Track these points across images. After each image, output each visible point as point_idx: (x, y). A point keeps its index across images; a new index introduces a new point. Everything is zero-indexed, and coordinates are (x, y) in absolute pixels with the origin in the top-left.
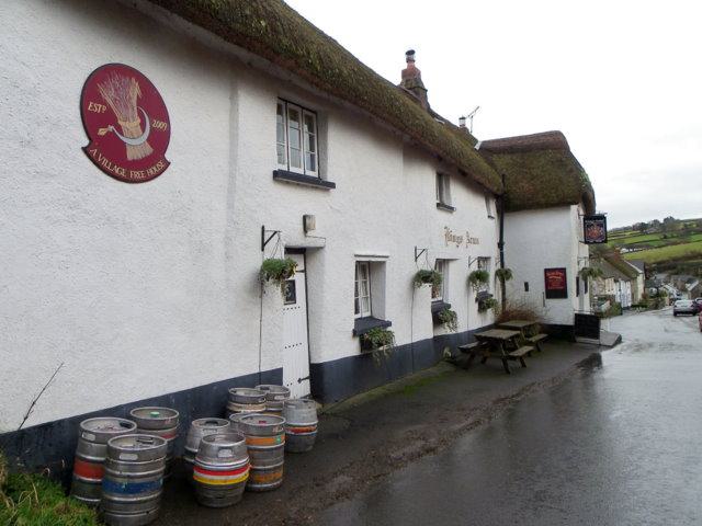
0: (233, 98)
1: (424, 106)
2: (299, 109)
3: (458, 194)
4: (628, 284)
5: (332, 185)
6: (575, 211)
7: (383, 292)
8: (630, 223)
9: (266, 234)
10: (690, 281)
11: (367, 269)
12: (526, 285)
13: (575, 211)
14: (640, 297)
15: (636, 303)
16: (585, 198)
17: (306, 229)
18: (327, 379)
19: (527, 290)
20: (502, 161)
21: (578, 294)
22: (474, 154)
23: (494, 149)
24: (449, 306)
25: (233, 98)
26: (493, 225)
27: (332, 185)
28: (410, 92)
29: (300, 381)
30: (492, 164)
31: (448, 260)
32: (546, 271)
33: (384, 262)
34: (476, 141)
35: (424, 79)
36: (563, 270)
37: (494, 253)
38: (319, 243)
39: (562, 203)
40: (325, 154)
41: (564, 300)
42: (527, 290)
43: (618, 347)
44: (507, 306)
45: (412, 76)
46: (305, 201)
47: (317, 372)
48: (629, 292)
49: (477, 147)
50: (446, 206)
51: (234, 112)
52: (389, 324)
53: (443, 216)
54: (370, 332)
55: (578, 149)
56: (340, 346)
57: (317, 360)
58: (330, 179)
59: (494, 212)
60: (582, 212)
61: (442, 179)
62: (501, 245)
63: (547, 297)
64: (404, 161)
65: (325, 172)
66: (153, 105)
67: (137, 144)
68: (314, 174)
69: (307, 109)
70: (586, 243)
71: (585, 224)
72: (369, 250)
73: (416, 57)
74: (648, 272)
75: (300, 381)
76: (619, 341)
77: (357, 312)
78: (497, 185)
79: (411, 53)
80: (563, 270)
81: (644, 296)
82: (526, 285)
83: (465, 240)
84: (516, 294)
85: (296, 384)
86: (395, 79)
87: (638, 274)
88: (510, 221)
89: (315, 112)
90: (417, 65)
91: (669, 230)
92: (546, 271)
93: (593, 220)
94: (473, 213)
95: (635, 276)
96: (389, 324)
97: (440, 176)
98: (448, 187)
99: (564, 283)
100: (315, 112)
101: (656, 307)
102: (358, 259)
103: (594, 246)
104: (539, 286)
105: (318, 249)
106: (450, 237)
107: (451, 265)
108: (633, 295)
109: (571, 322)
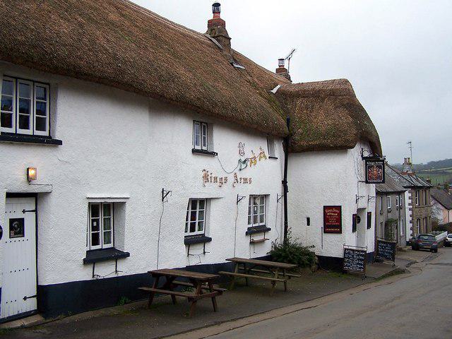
2: (31, 83)
3: (226, 142)
5: (60, 143)
7: (123, 227)
9: (165, 192)
12: (308, 219)
16: (370, 140)
19: (308, 224)
21: (354, 229)
27: (60, 143)
28: (212, 39)
29: (25, 298)
32: (325, 208)
35: (230, 29)
36: (339, 208)
38: (47, 189)
39: (341, 147)
40: (55, 117)
41: (339, 235)
42: (308, 224)
44: (34, 200)
45: (217, 27)
53: (203, 162)
57: (44, 283)
58: (57, 137)
60: (366, 154)
62: (285, 182)
64: (150, 111)
65: (54, 132)
68: (45, 133)
69: (36, 82)
71: (366, 165)
73: (222, 8)
75: (25, 298)
77: (95, 240)
80: (339, 208)
82: (308, 219)
86: (202, 28)
89: (48, 84)
90: (222, 16)
92: (325, 208)
93: (375, 158)
99: (339, 219)
100: (48, 84)
102: (91, 201)
103: (378, 185)
105: (47, 194)
107: (213, 205)
109: (341, 256)
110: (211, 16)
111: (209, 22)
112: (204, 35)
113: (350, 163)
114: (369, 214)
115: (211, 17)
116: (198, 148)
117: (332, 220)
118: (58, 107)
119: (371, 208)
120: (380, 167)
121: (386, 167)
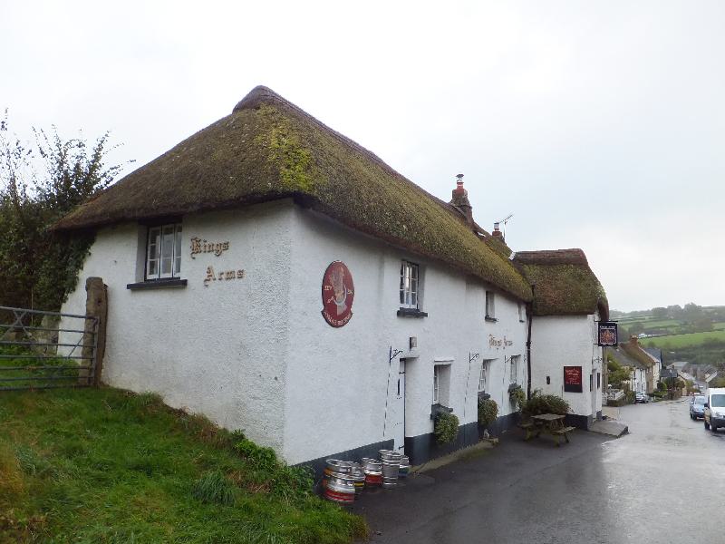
0: (381, 268)
1: (469, 221)
4: (644, 373)
5: (426, 315)
6: (593, 319)
8: (648, 307)
10: (710, 372)
11: (440, 369)
12: (548, 379)
13: (593, 319)
14: (655, 386)
15: (651, 392)
16: (601, 307)
17: (411, 346)
18: (417, 447)
19: (548, 383)
20: (533, 271)
22: (507, 266)
23: (526, 260)
24: (489, 396)
25: (381, 268)
26: (523, 327)
27: (426, 315)
30: (523, 274)
31: (490, 360)
33: (450, 365)
34: (509, 251)
36: (579, 369)
37: (523, 351)
39: (581, 313)
42: (548, 383)
43: (626, 437)
45: (459, 195)
46: (411, 328)
47: (409, 442)
48: (644, 380)
49: (511, 257)
50: (490, 319)
51: (381, 276)
52: (452, 410)
53: (489, 327)
54: (440, 415)
55: (594, 265)
56: (422, 427)
57: (411, 435)
59: (524, 317)
61: (489, 296)
62: (528, 344)
63: (566, 391)
64: (467, 288)
66: (348, 283)
67: (341, 306)
70: (600, 345)
72: (442, 358)
74: (665, 360)
76: (625, 432)
78: (529, 296)
79: (460, 176)
80: (579, 369)
81: (660, 385)
82: (548, 379)
83: (503, 344)
84: (539, 386)
85: (399, 443)
86: (447, 198)
87: (654, 363)
88: (537, 324)
91: (694, 317)
93: (605, 321)
94: (510, 317)
95: (650, 365)
96: (452, 410)
97: (487, 293)
98: (492, 302)
99: (580, 379)
101: (672, 397)
102: (437, 364)
104: (558, 381)
106: (493, 342)
108: (648, 383)
110: (702, 425)
111: (454, 192)
112: (449, 205)
113: (586, 328)
114: (599, 374)
115: (456, 188)
116: (406, 306)
117: (573, 380)
118: (426, 293)
119: (600, 370)
120: (613, 331)
121: (73, 355)
